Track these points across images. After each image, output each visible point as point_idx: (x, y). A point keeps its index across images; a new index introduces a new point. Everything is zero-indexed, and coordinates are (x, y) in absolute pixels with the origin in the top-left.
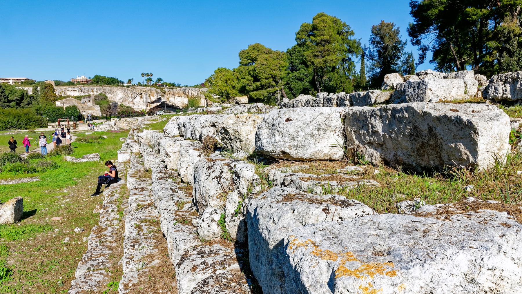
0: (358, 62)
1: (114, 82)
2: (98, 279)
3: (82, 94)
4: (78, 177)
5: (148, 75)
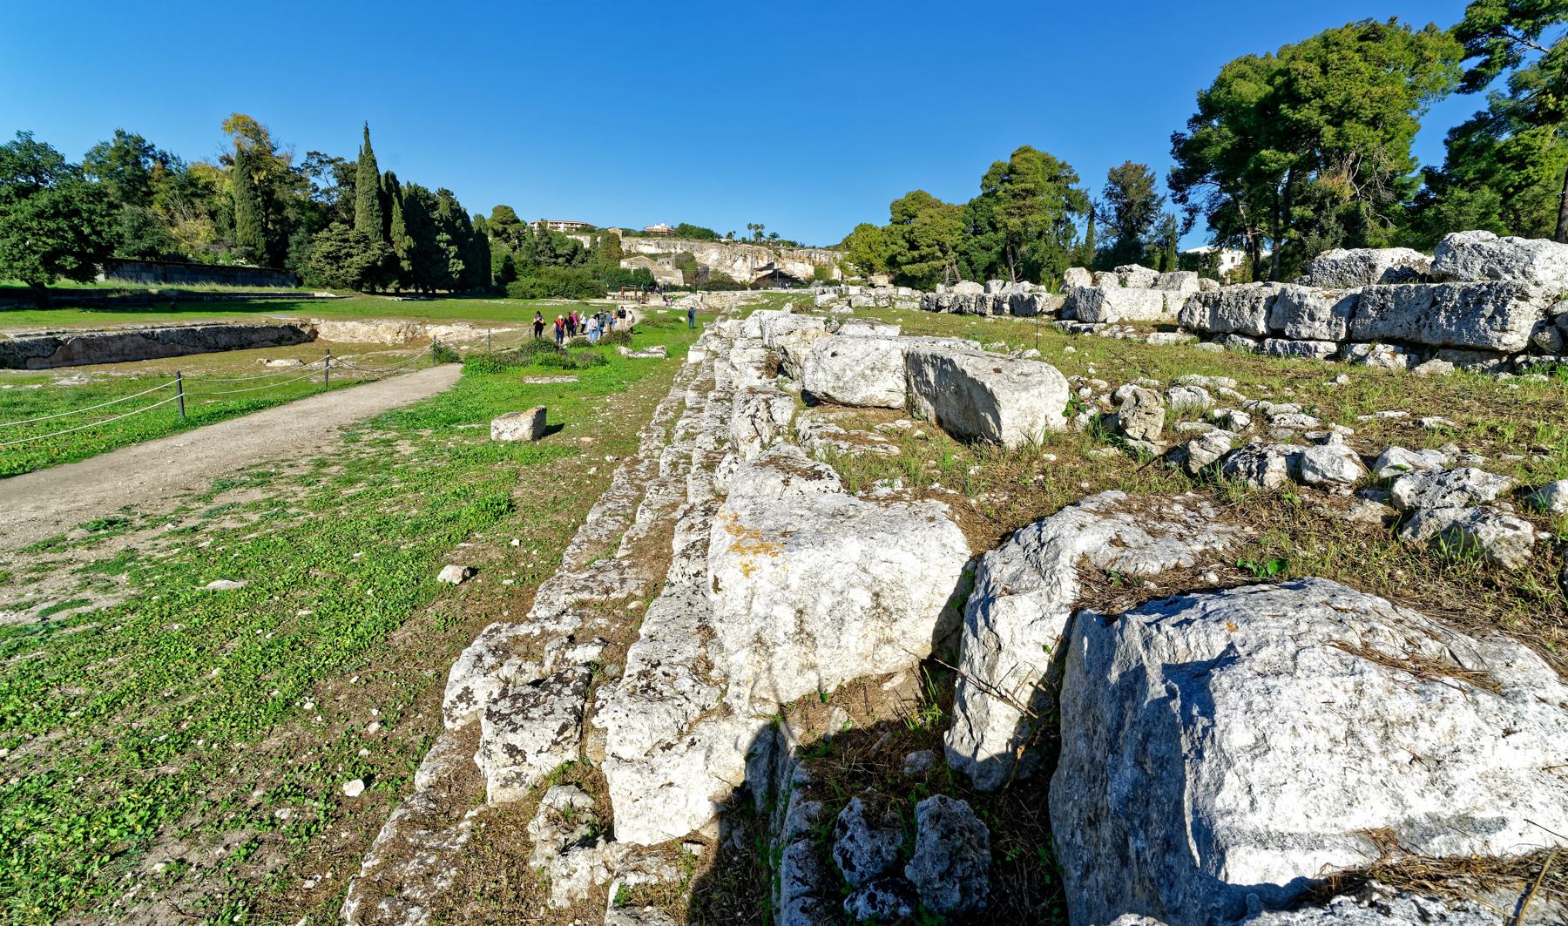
0: (1080, 226)
1: (708, 236)
2: (611, 528)
3: (660, 251)
4: (630, 380)
5: (757, 227)
